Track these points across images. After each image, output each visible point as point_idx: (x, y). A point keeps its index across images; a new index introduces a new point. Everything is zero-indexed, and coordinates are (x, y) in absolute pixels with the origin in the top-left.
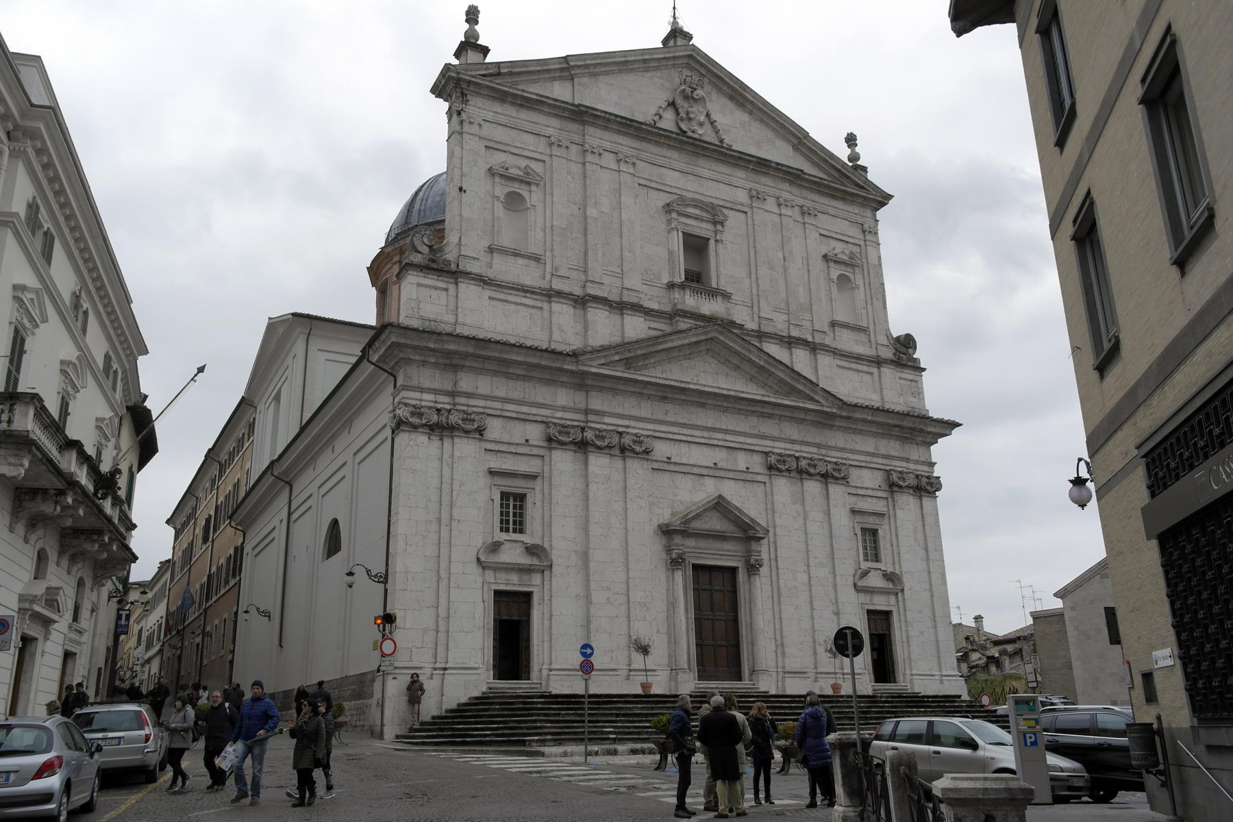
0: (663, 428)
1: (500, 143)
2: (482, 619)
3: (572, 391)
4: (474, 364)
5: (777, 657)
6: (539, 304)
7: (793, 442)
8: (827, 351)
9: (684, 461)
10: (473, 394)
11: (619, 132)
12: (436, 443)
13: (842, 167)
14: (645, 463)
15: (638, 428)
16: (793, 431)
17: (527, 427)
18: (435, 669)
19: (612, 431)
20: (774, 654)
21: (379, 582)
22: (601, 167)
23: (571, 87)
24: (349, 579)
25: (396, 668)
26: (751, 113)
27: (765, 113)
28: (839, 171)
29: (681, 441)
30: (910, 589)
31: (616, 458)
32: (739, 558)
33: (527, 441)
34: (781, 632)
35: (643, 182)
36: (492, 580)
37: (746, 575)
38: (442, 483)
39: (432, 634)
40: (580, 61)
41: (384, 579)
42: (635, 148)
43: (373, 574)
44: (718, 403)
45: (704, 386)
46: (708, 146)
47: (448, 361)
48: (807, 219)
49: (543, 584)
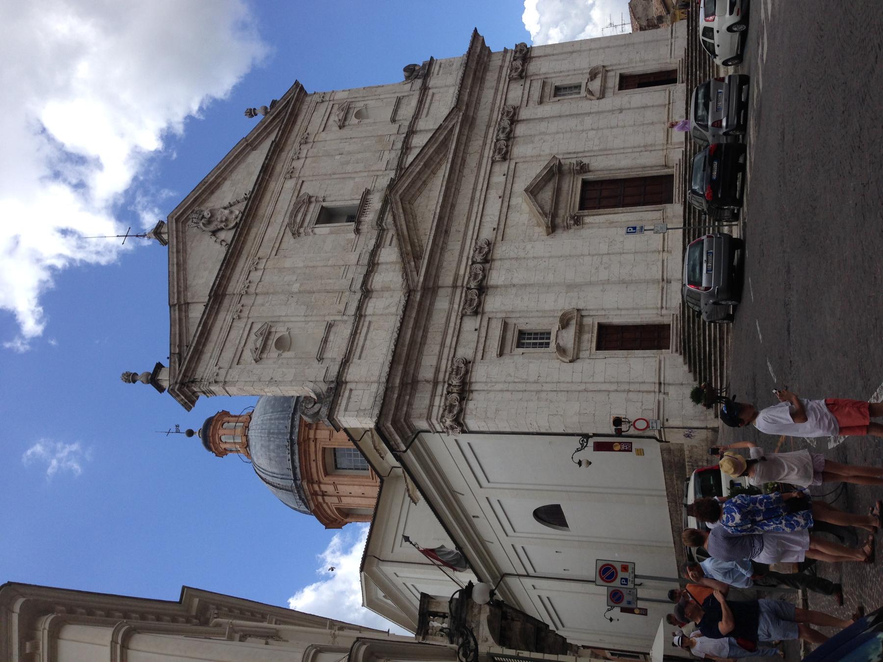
0: (470, 233)
1: (235, 354)
2: (620, 359)
5: (655, 150)
6: (366, 324)
7: (485, 144)
8: (414, 123)
9: (497, 219)
10: (436, 368)
11: (233, 269)
12: (475, 395)
14: (497, 245)
15: (469, 250)
16: (476, 145)
17: (465, 330)
18: (660, 391)
19: (471, 269)
20: (652, 152)
22: (260, 282)
23: (195, 305)
29: (481, 221)
30: (603, 61)
32: (575, 179)
33: (476, 330)
34: (635, 147)
35: (274, 253)
36: (588, 352)
37: (588, 173)
38: (508, 391)
39: (631, 395)
42: (247, 258)
44: (452, 195)
45: (438, 202)
47: (409, 387)
49: (592, 316)
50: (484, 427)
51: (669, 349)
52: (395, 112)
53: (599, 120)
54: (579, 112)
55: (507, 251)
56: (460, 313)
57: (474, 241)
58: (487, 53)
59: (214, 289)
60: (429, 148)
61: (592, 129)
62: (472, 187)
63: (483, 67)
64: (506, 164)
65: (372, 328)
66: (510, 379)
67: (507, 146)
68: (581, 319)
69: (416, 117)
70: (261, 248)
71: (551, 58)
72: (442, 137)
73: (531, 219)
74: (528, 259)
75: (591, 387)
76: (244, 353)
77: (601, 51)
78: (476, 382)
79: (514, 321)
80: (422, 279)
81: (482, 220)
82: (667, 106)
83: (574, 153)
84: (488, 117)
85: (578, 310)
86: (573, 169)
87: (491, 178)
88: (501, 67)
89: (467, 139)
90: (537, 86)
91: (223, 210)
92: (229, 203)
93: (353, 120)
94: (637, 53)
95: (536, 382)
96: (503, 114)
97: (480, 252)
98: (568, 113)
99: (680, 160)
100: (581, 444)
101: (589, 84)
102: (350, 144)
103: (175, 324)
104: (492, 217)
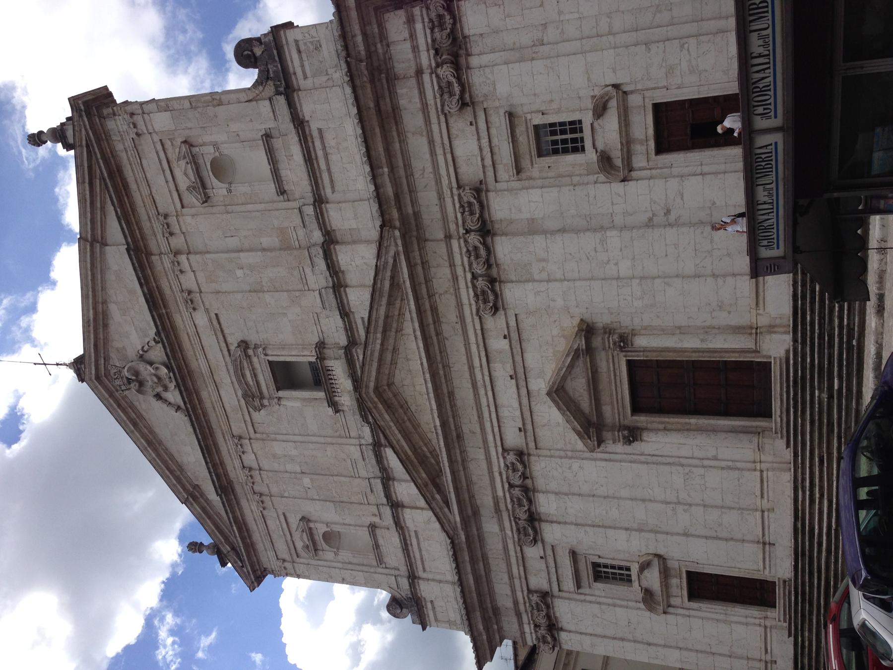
0: (490, 438)
6: (413, 534)
9: (518, 413)
13: (84, 182)
15: (498, 463)
26: (105, 302)
27: (94, 291)
28: (91, 184)
40: (178, 490)
44: (443, 380)
59: (217, 486)
60: (377, 310)
85: (616, 86)
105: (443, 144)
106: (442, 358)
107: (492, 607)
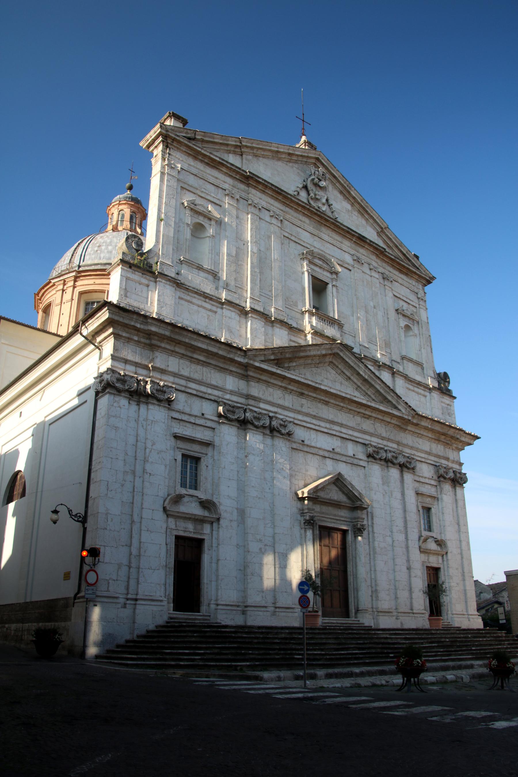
0: (300, 417)
1: (191, 186)
2: (165, 559)
3: (237, 379)
4: (168, 347)
5: (372, 600)
6: (214, 309)
7: (383, 438)
8: (401, 376)
9: (313, 444)
10: (165, 371)
11: (272, 197)
12: (134, 407)
14: (288, 443)
15: (283, 414)
16: (382, 430)
17: (204, 404)
18: (128, 599)
19: (265, 414)
20: (370, 598)
21: (78, 521)
22: (260, 218)
23: (240, 160)
24: (55, 517)
25: (97, 596)
29: (311, 429)
30: (451, 552)
31: (267, 437)
32: (348, 523)
33: (203, 414)
34: (376, 581)
35: (286, 235)
36: (173, 527)
37: (353, 536)
38: (137, 441)
39: (125, 569)
41: (83, 520)
42: (282, 210)
43: (74, 514)
44: (337, 403)
45: (331, 388)
46: (329, 219)
47: (148, 342)
48: (386, 283)
49: (212, 533)
50: (101, 414)
51: (173, 610)
52: (411, 360)
53: (402, 547)
54: (409, 529)
55: (281, 451)
56: (220, 400)
57: (292, 420)
58: (460, 447)
61: (393, 541)
62: (344, 423)
63: (447, 442)
64: (364, 457)
65: (210, 313)
66: (149, 445)
67: (380, 459)
68: (209, 521)
69: (406, 378)
70: (291, 224)
71: (455, 505)
72: (390, 398)
73: (311, 478)
74: (273, 472)
75: (135, 527)
76: (192, 195)
77: (459, 551)
78: (148, 409)
79: (210, 454)
80: (257, 364)
81: (312, 430)
82: (411, 611)
83: (373, 523)
84: (406, 443)
85: (218, 519)
86: (358, 521)
87: (351, 442)
88: (447, 459)
89: (388, 422)
90: (432, 491)
91: (326, 197)
92: (332, 205)
93: (403, 322)
94: (458, 584)
95: (144, 471)
96: (408, 457)
97: (281, 425)
98: (408, 518)
99: (363, 624)
100: (76, 514)
101: (433, 539)
102: (383, 317)
103: (224, 140)
104: (315, 440)
105: (428, 459)
106: (347, 408)
107: (159, 347)
